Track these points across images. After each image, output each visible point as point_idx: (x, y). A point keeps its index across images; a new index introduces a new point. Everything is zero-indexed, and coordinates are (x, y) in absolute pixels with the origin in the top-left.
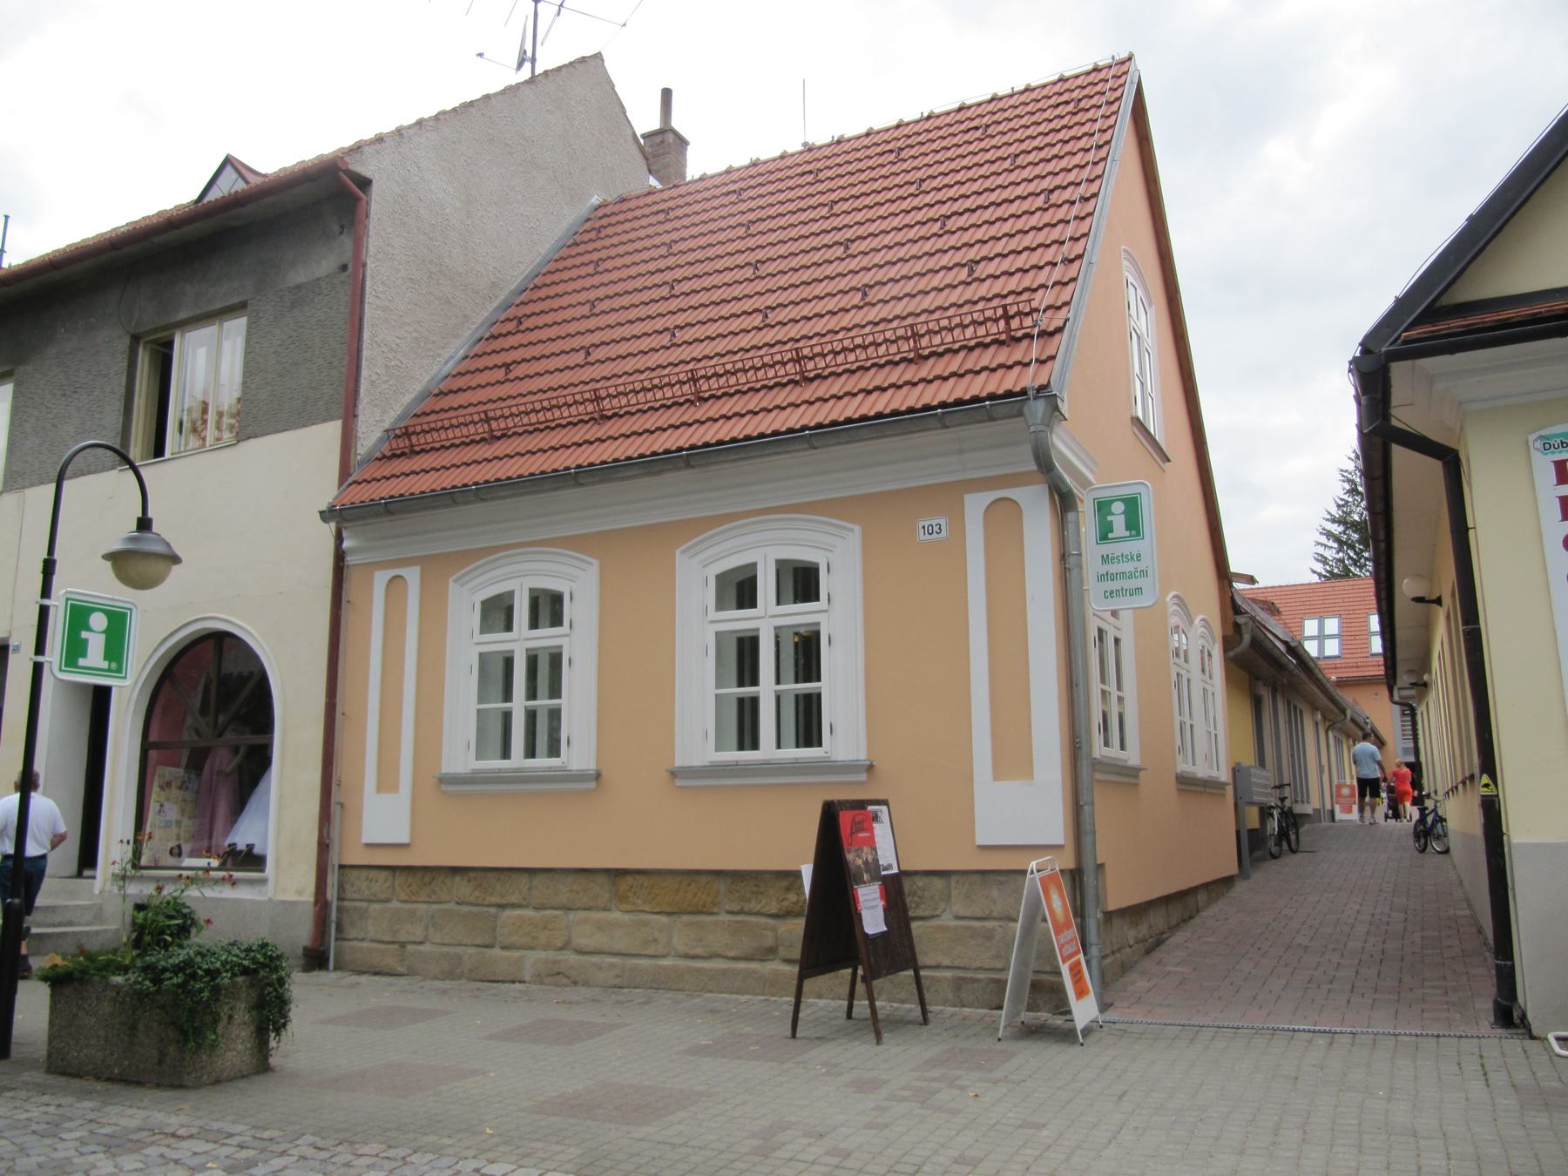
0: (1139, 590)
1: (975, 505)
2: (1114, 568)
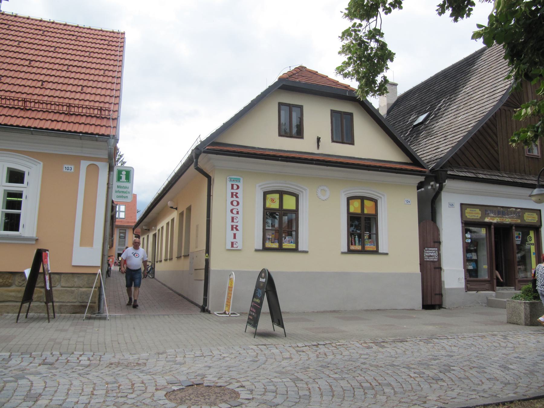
0: (127, 197)
1: (84, 165)
2: (121, 190)
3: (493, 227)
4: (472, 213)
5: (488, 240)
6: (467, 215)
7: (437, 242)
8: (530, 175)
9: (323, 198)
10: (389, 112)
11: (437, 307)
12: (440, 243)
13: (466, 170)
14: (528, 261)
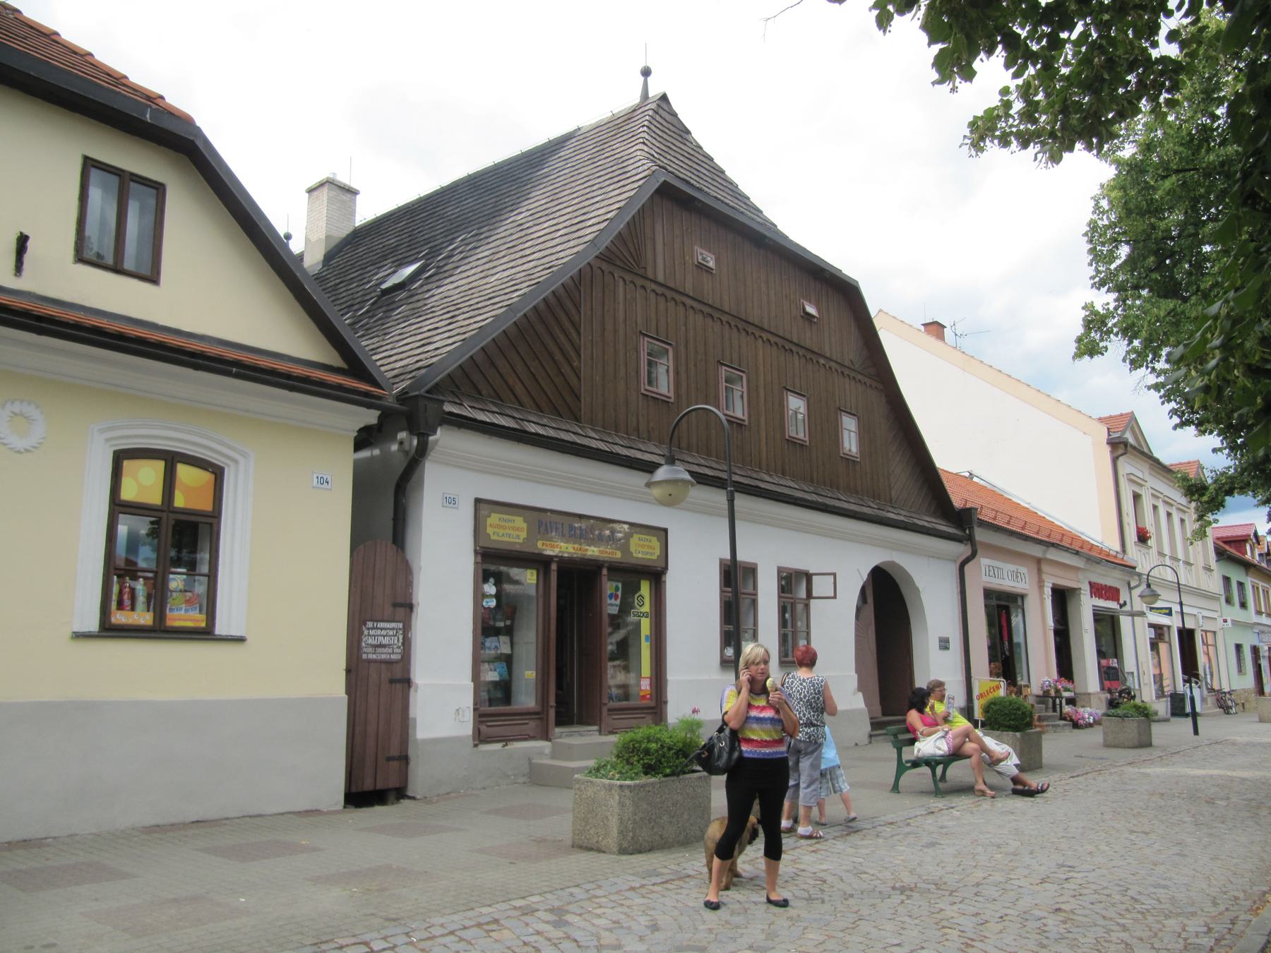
3: (554, 567)
4: (504, 527)
5: (541, 601)
6: (490, 530)
7: (401, 605)
8: (649, 440)
9: (20, 443)
10: (328, 257)
11: (392, 796)
12: (410, 607)
13: (495, 409)
14: (632, 651)
